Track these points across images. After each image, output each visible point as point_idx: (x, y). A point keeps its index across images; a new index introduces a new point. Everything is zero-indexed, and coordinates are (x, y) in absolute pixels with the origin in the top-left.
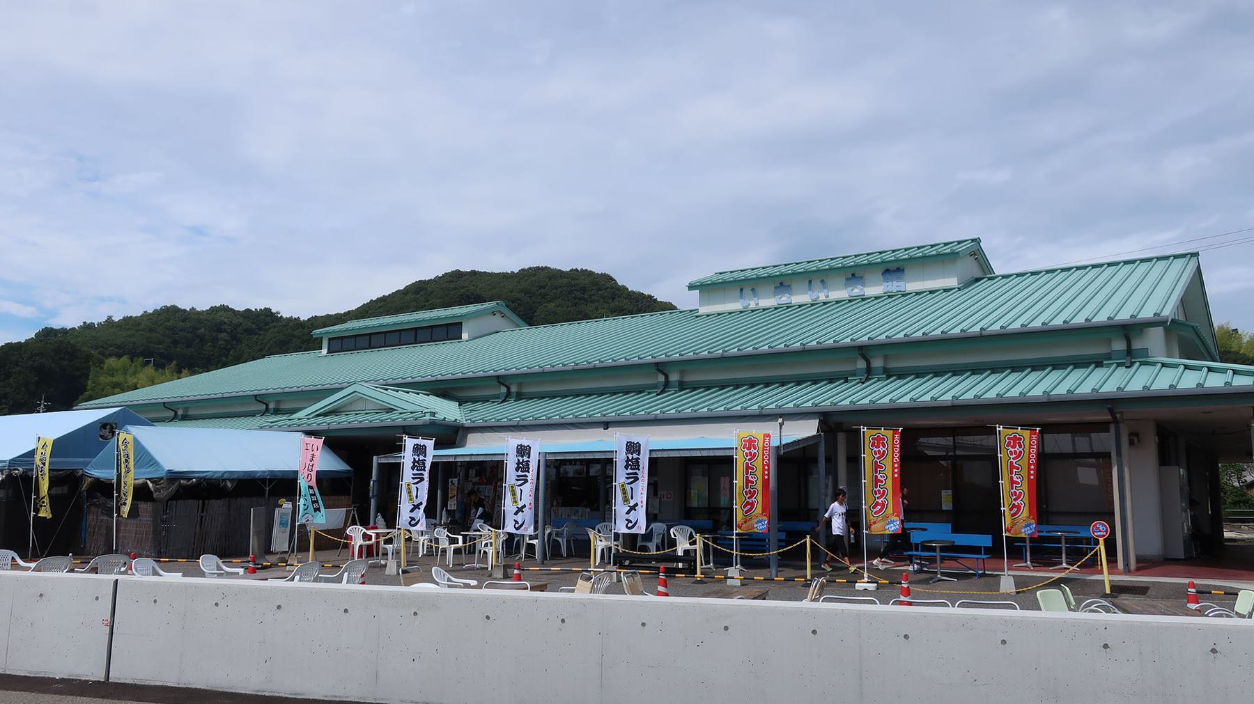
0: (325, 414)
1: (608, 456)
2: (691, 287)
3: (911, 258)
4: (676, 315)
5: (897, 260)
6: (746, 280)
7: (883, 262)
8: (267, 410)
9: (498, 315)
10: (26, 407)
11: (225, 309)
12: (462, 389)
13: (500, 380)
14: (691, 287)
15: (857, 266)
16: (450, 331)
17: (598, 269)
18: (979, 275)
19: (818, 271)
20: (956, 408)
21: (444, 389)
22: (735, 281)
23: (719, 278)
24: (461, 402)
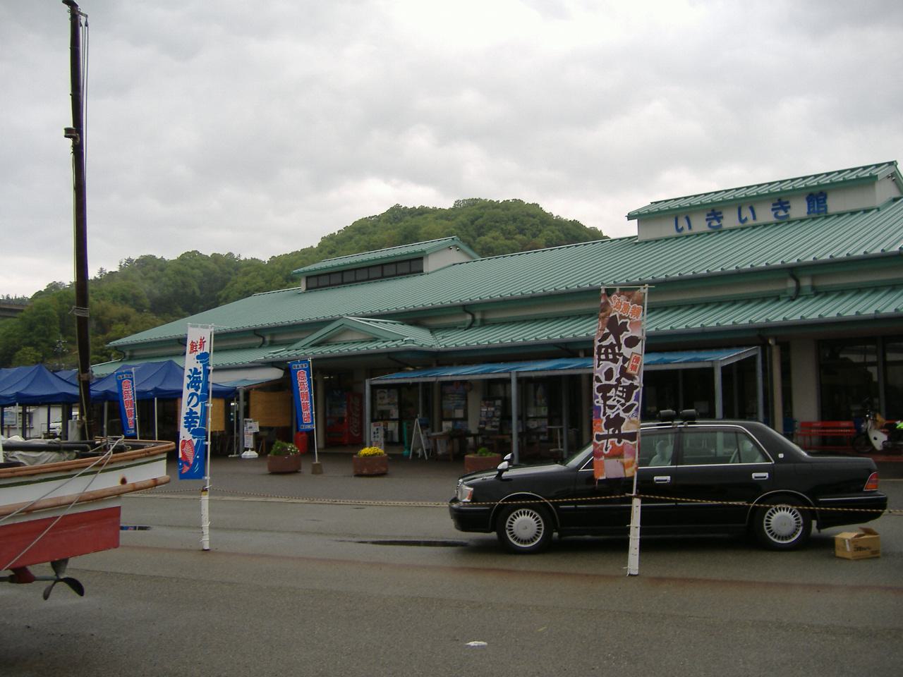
0: (318, 345)
1: (566, 366)
2: (630, 217)
3: (832, 183)
4: (599, 245)
5: (819, 185)
6: (681, 208)
7: (807, 188)
8: (264, 342)
9: (454, 250)
10: (852, 532)
11: (518, 202)
12: (430, 318)
13: (466, 308)
14: (630, 217)
15: (782, 191)
16: (412, 266)
17: (223, 252)
18: (897, 195)
19: (747, 197)
20: (877, 320)
21: (414, 318)
22: (670, 210)
23: (655, 208)
24: (433, 330)
